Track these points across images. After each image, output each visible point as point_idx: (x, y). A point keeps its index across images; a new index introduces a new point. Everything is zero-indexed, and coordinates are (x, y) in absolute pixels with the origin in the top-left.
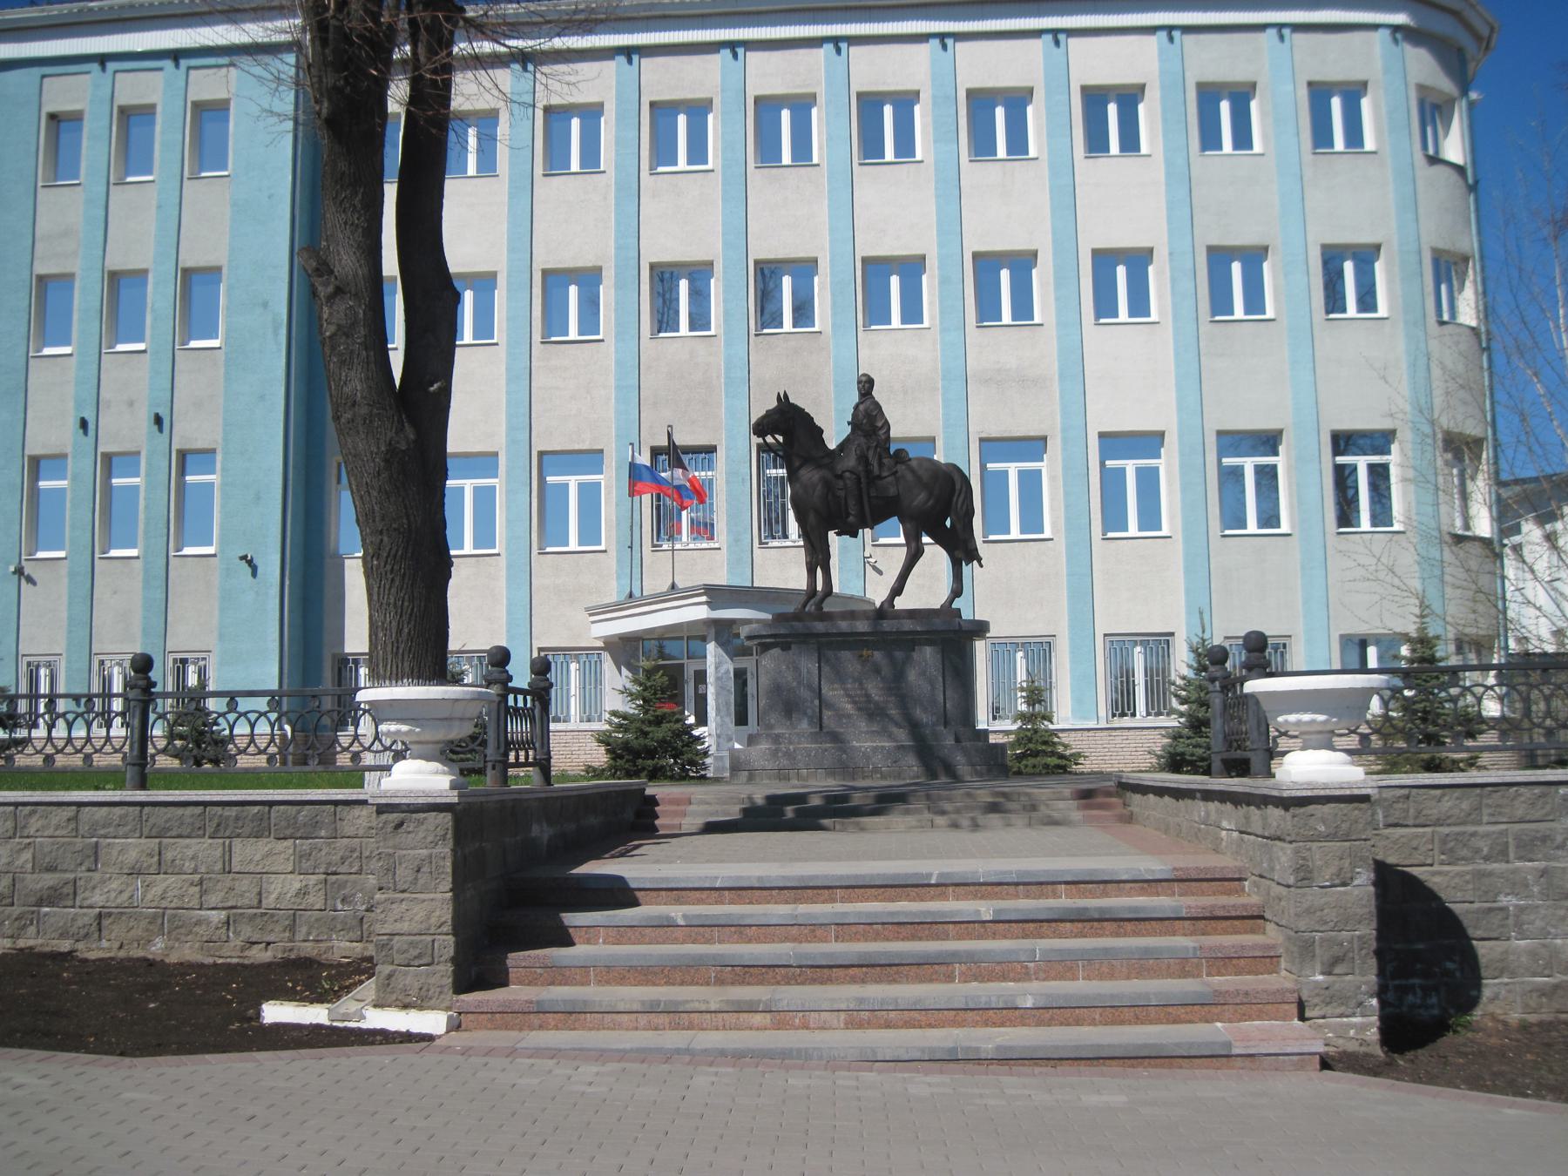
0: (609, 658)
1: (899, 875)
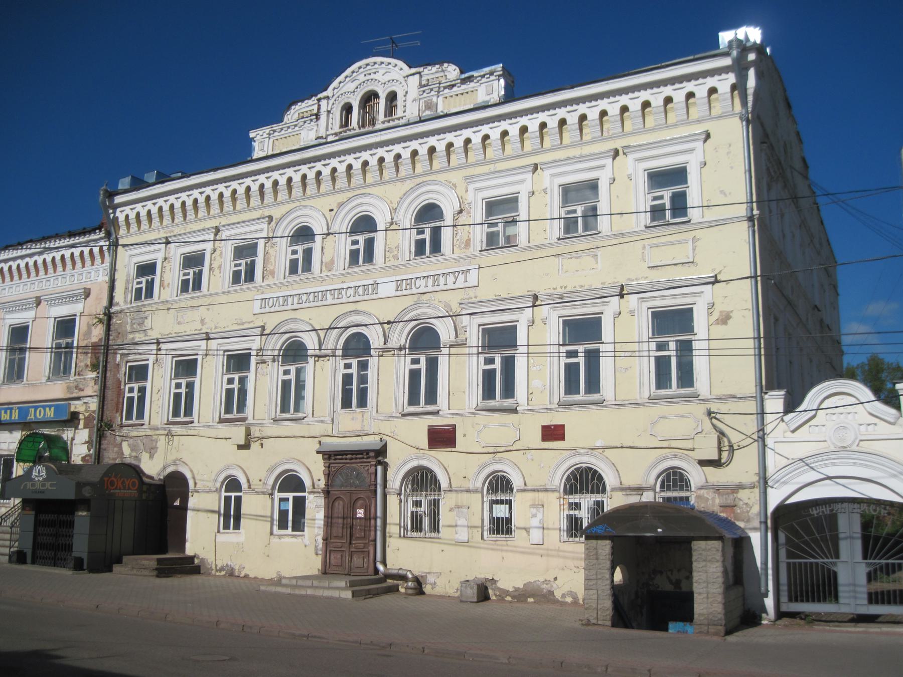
0: (740, 522)
1: (693, 322)
